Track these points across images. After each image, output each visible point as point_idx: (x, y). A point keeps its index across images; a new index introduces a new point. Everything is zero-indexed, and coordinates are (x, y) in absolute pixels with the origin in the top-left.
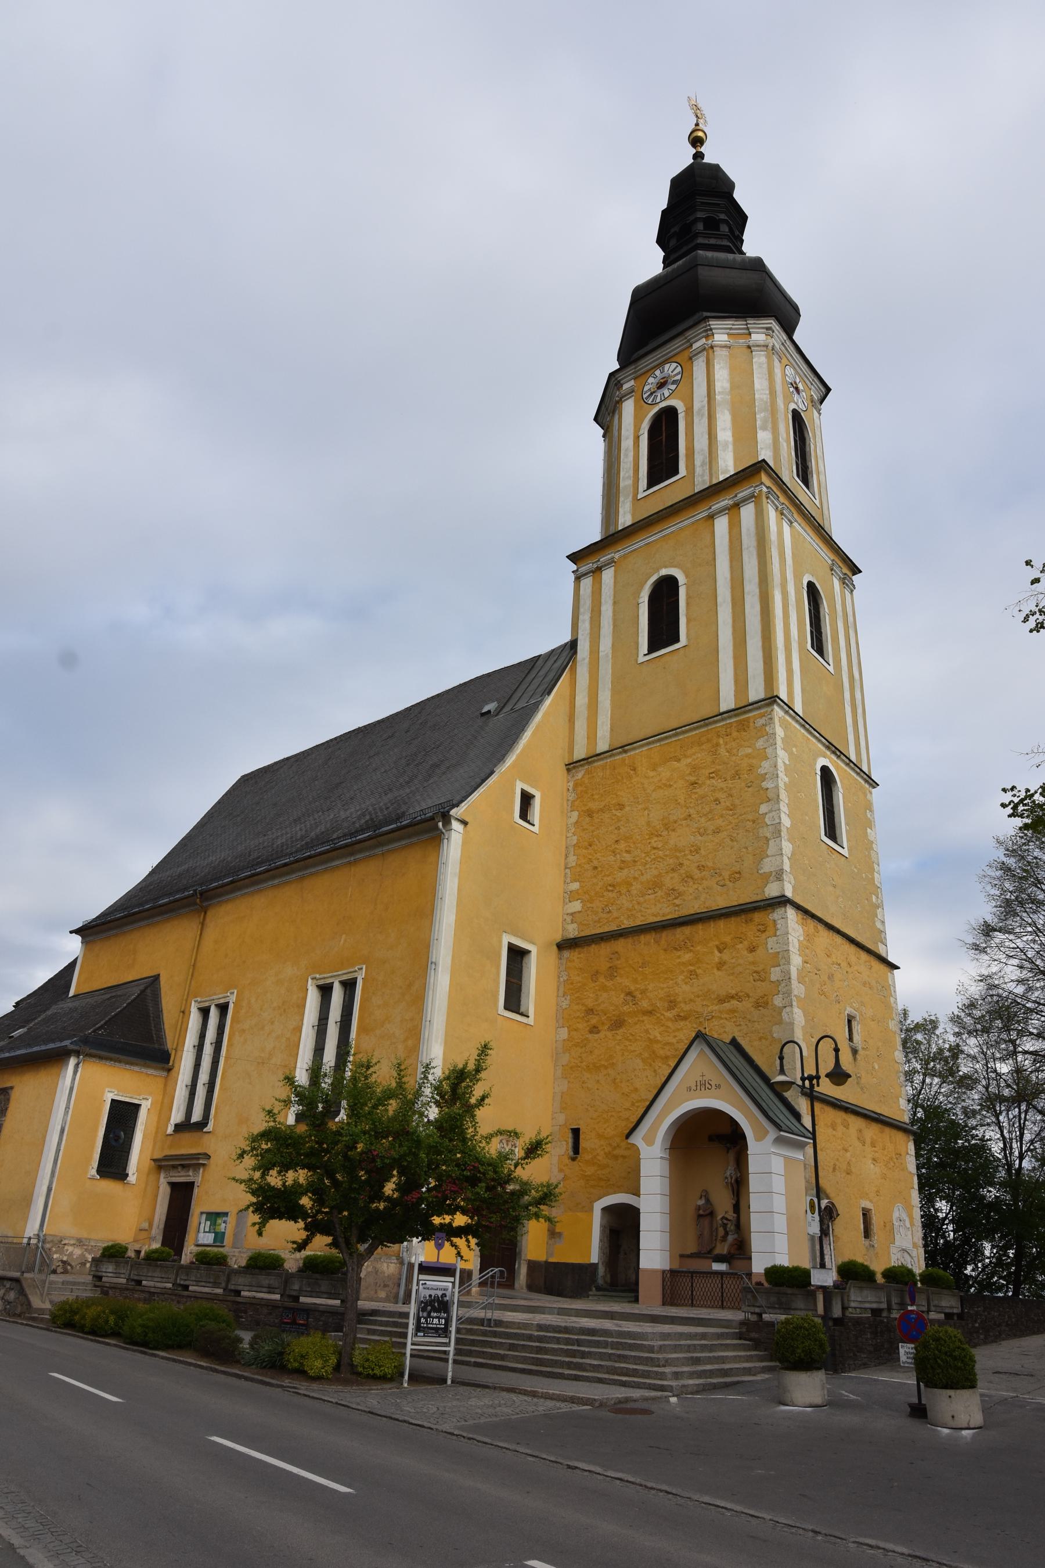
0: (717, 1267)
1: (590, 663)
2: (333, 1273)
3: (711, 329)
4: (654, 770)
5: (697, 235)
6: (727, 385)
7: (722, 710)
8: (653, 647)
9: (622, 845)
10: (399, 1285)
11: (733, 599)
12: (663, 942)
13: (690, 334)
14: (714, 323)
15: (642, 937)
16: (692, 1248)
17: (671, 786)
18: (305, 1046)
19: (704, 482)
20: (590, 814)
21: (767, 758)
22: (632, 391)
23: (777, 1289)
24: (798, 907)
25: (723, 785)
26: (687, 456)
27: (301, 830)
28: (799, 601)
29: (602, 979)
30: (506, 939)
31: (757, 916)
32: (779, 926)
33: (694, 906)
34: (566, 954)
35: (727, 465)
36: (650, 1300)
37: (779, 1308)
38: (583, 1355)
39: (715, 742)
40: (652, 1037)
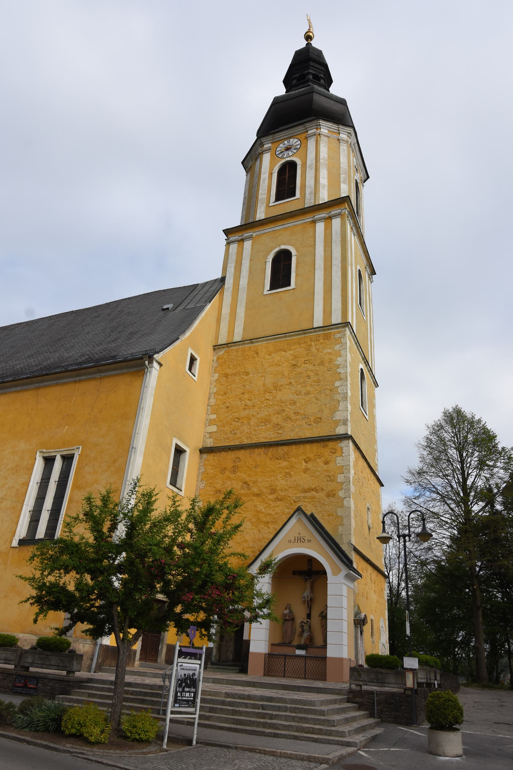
0: (299, 652)
1: (233, 290)
2: (61, 651)
3: (320, 125)
4: (270, 355)
5: (309, 80)
6: (326, 156)
7: (314, 327)
8: (273, 286)
9: (246, 396)
10: (92, 660)
11: (325, 267)
12: (270, 454)
13: (308, 125)
14: (322, 122)
15: (256, 450)
16: (278, 641)
17: (280, 365)
18: (30, 495)
19: (310, 202)
20: (226, 376)
21: (341, 356)
22: (269, 149)
23: (375, 670)
24: (354, 442)
25: (313, 368)
26: (301, 188)
27: (34, 361)
28: (356, 277)
29: (227, 473)
30: (175, 441)
31: (331, 444)
32: (344, 451)
33: (292, 436)
34: (205, 456)
35: (324, 197)
36: (256, 671)
37: (377, 682)
38: (272, 717)
39: (309, 343)
40: (259, 510)
